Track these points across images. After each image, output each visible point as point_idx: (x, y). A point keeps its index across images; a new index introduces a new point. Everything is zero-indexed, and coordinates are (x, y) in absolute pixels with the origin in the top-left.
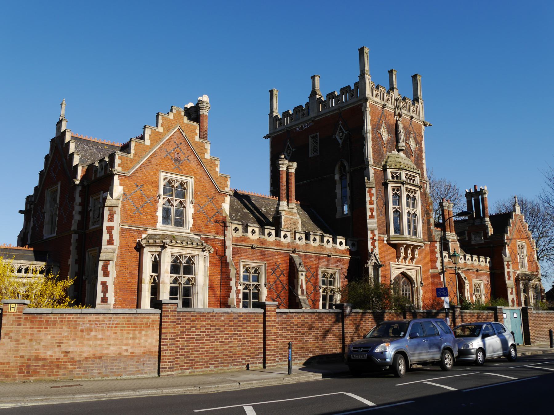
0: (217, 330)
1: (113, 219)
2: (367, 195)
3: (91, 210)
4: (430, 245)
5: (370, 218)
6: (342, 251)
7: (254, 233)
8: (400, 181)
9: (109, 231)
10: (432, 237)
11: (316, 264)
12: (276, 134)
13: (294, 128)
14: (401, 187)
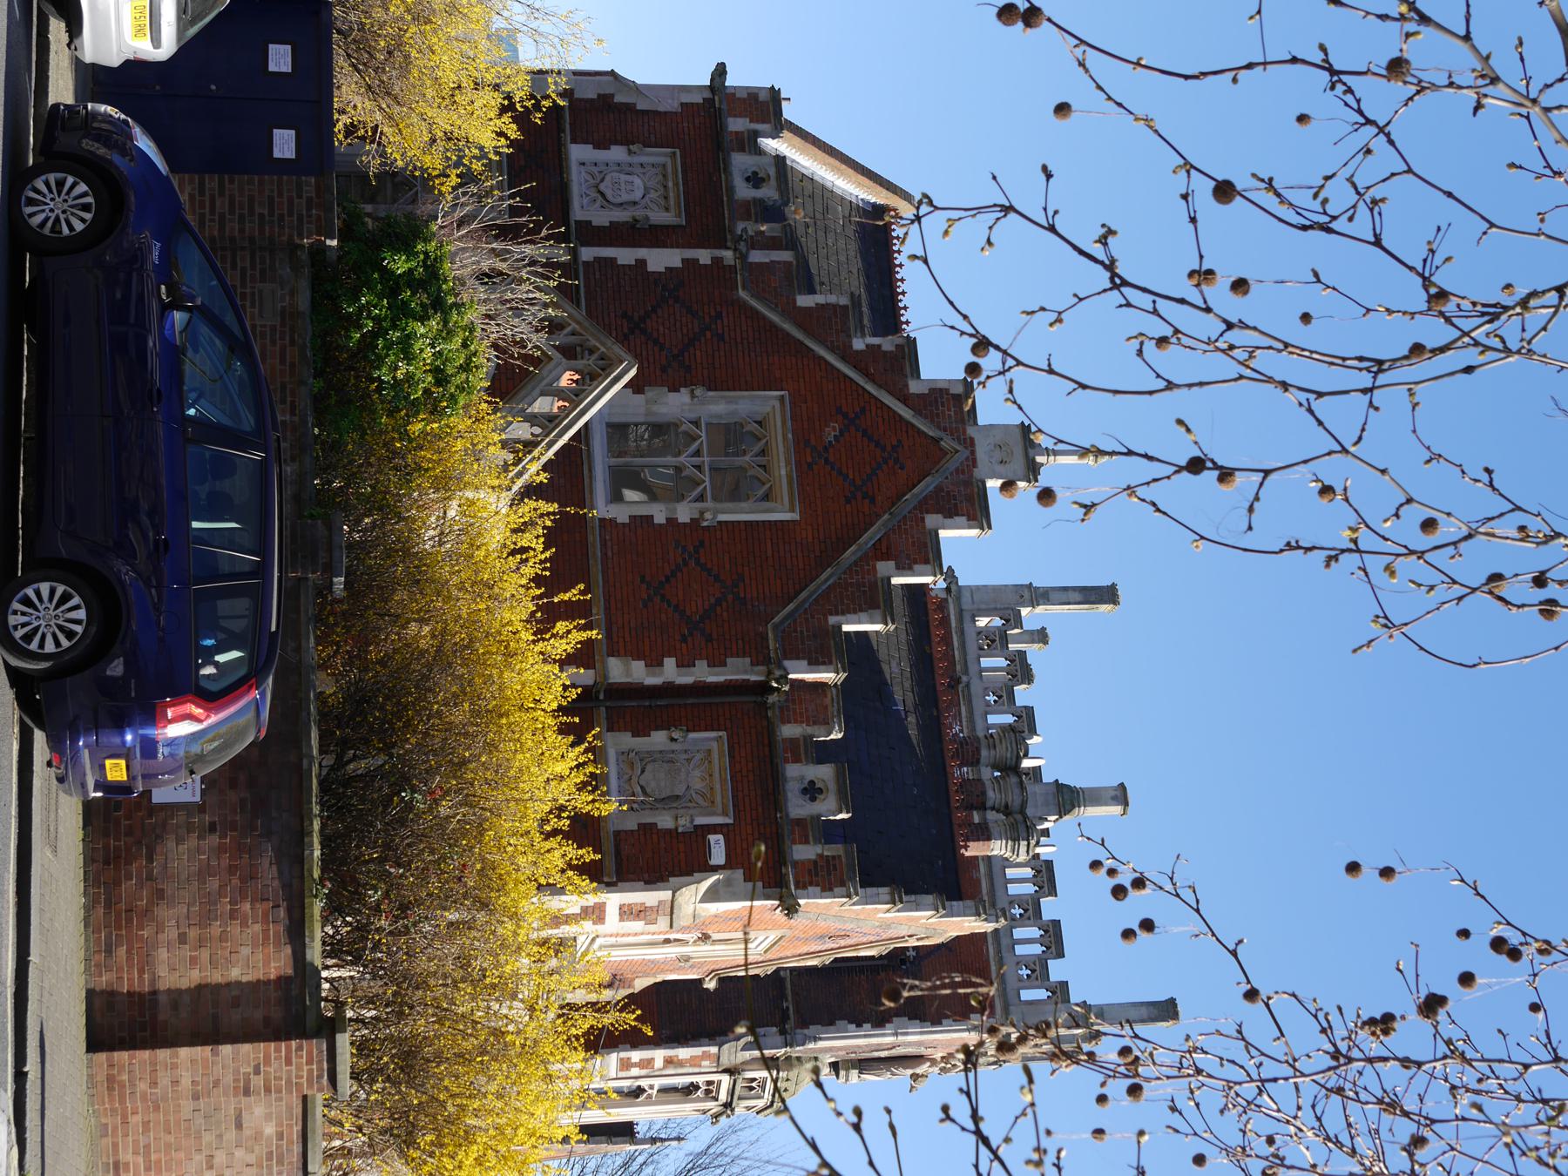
1: (628, 920)
2: (697, 1051)
3: (673, 740)
5: (622, 1059)
8: (736, 1097)
9: (590, 910)
12: (953, 625)
13: (963, 709)
14: (717, 1100)
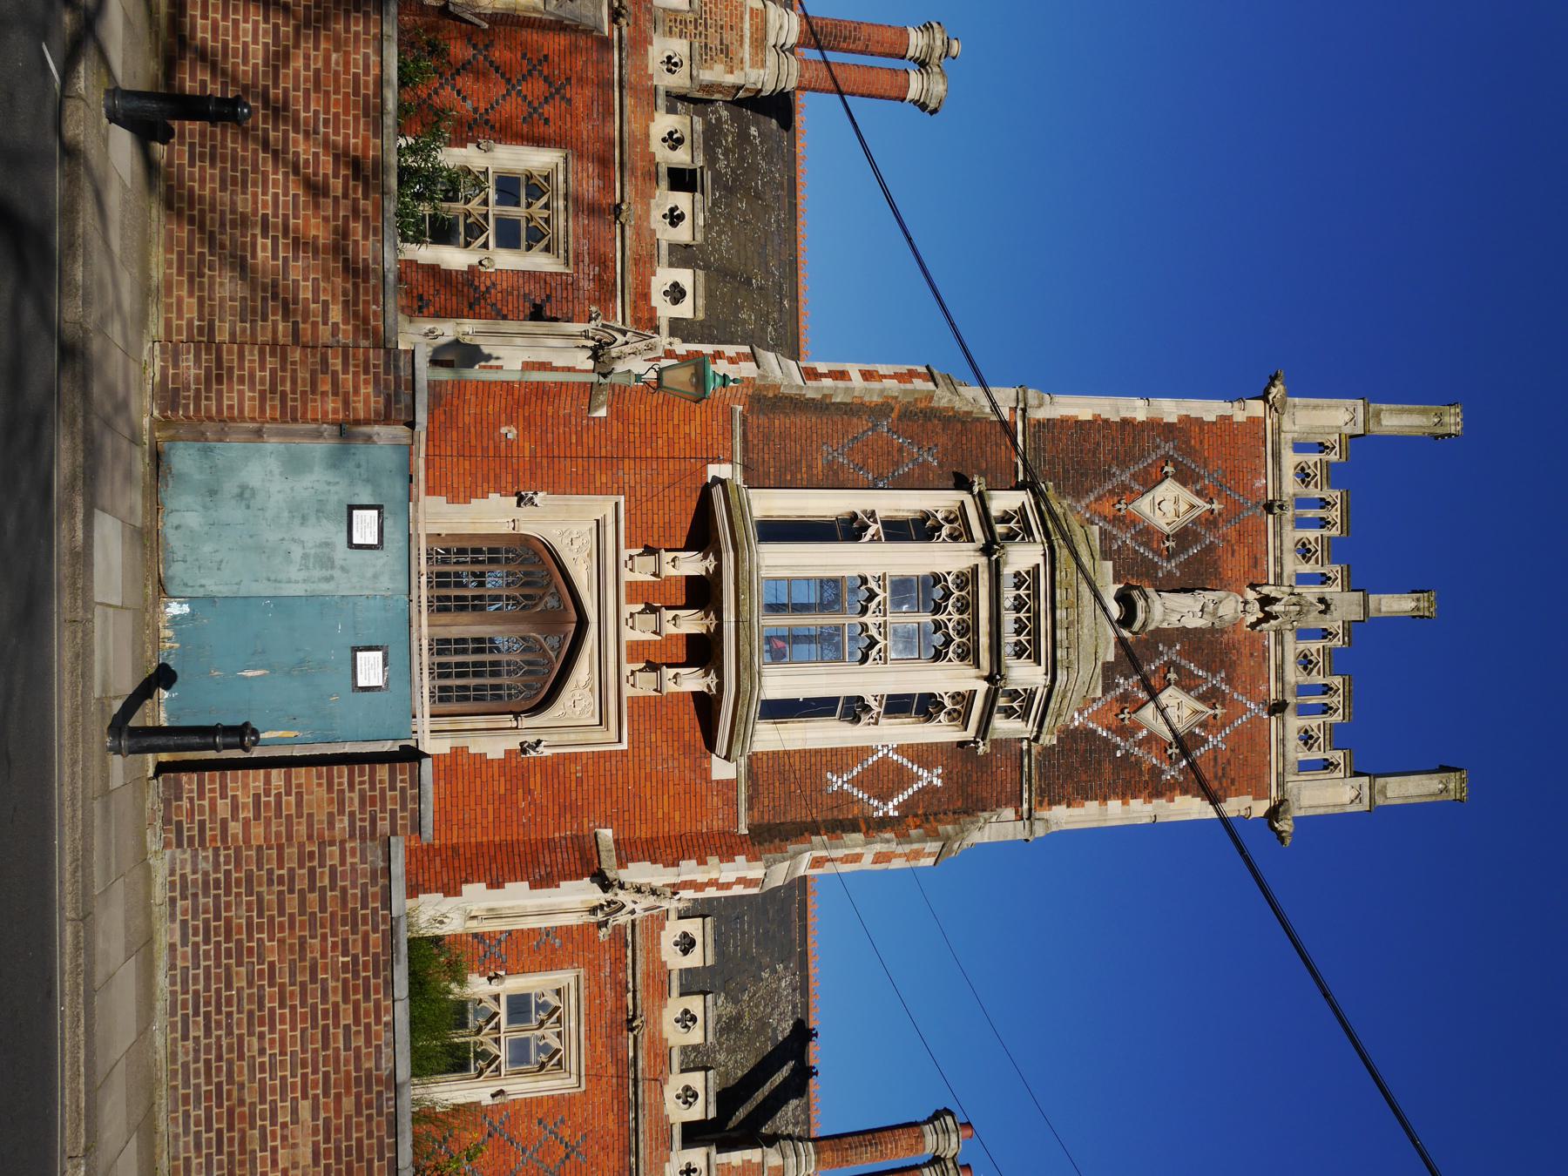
0: (328, 1043)
4: (734, 835)
6: (646, 296)
7: (685, 1102)
10: (777, 841)
11: (579, 133)
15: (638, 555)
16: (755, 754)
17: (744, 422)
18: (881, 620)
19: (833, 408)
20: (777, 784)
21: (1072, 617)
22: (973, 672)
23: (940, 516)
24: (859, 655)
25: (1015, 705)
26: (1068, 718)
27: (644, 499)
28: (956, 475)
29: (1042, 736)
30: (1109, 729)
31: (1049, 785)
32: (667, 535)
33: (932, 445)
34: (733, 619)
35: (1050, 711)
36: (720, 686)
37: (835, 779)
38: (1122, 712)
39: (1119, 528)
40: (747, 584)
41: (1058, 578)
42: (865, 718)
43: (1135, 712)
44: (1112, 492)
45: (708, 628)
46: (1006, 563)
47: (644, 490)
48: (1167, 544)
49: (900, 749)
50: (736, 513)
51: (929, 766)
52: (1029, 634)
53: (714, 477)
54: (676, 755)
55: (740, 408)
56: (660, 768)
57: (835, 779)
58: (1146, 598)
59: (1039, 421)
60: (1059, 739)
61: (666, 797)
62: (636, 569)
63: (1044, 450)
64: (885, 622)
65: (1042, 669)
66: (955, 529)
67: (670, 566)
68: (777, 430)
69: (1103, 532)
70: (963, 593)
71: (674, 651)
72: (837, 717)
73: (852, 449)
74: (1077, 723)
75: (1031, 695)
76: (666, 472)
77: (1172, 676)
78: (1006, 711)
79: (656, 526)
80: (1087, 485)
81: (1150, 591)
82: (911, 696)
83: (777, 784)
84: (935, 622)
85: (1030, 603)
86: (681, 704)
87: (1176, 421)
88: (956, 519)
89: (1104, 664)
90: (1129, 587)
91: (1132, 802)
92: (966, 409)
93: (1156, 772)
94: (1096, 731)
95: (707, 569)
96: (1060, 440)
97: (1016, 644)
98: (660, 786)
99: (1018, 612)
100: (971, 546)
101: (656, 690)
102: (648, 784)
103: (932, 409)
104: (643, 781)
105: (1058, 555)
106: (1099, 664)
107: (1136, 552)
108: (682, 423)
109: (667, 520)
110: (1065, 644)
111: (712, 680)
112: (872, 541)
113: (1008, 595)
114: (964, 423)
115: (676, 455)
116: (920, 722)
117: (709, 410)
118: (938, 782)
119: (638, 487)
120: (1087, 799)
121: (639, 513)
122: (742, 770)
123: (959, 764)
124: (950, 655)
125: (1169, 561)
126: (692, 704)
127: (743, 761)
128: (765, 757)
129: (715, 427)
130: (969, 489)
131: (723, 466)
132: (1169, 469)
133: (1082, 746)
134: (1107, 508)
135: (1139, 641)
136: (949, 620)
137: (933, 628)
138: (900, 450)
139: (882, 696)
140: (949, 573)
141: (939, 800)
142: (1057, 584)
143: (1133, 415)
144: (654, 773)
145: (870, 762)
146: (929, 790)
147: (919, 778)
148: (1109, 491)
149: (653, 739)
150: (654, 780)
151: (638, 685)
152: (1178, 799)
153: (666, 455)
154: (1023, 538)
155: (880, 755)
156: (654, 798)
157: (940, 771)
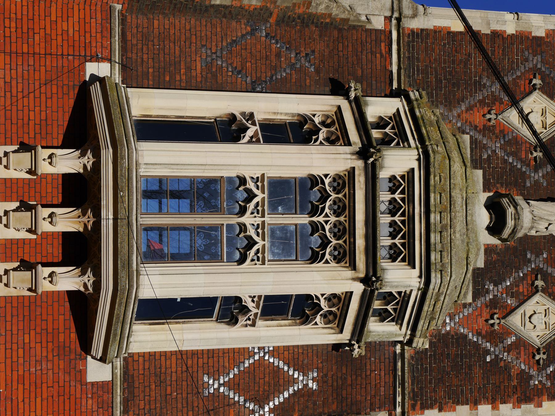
15: (14, 152)
16: (131, 355)
17: (123, 21)
18: (259, 220)
19: (212, 10)
20: (153, 387)
21: (446, 221)
22: (350, 273)
23: (317, 120)
24: (237, 256)
25: (389, 308)
26: (440, 322)
27: (20, 95)
28: (332, 81)
29: (416, 340)
30: (479, 334)
31: (421, 388)
32: (44, 132)
33: (309, 51)
34: (111, 216)
35: (424, 314)
36: (97, 285)
37: (211, 382)
38: (492, 318)
39: (489, 138)
40: (125, 180)
41: (432, 182)
42: (242, 320)
43: (504, 318)
44: (482, 102)
45: (85, 226)
46: (382, 167)
47: (20, 86)
48: (535, 154)
49: (276, 352)
50: (116, 111)
51: (303, 370)
52: (403, 237)
53: (92, 76)
54: (50, 357)
55: (119, 7)
56: (33, 370)
57: (211, 382)
58: (516, 205)
59: (412, 31)
60: (431, 343)
61: (39, 400)
62: (11, 166)
63: (418, 59)
64: (263, 222)
65: (416, 272)
66: (332, 133)
67: (46, 163)
68: (156, 31)
69: (473, 141)
70: (340, 196)
71: (50, 251)
72: (214, 319)
73: (230, 52)
74: (448, 328)
75: (405, 297)
76: (43, 69)
77: (539, 283)
78: (380, 315)
79: (32, 123)
80: (459, 94)
81: (519, 199)
82: (287, 298)
83: (153, 387)
84: (312, 224)
85: (405, 207)
86: (56, 305)
87: (543, 35)
88: (333, 123)
89: (474, 270)
90: (498, 195)
91: (502, 407)
92: (343, 16)
93: (524, 377)
94: (466, 336)
95: (85, 167)
96: (433, 50)
97: (391, 247)
98: (33, 389)
99: (393, 215)
100: (347, 149)
101: (30, 290)
102: (21, 386)
103: (310, 15)
104: (15, 383)
105: (432, 160)
106: (471, 268)
107: (505, 161)
108: (59, 20)
109: (43, 117)
110: (439, 247)
111: (89, 278)
112: (250, 142)
113: (384, 197)
114: (340, 30)
115: (54, 51)
116: (296, 324)
117: (87, 7)
118: (313, 386)
119: (14, 83)
120: (458, 404)
121: (14, 108)
122: (118, 372)
123: (334, 368)
124: (327, 256)
125: (536, 171)
126: (67, 305)
127: (118, 363)
128: (141, 359)
129: (93, 24)
130: (345, 94)
131: (101, 64)
132: (537, 81)
133: (453, 350)
134: (477, 118)
135: (507, 248)
136: (326, 222)
137: (310, 230)
138: (278, 55)
139: (260, 297)
140: (326, 176)
141: (315, 404)
142: (432, 188)
143: (503, 28)
144: (27, 375)
145: (247, 365)
146: (305, 392)
147: (295, 381)
148: (480, 101)
149: (27, 341)
150: (27, 382)
151: (12, 284)
152: (546, 404)
153: (43, 52)
154: (398, 144)
155: (257, 357)
156: (27, 401)
157: (315, 375)
